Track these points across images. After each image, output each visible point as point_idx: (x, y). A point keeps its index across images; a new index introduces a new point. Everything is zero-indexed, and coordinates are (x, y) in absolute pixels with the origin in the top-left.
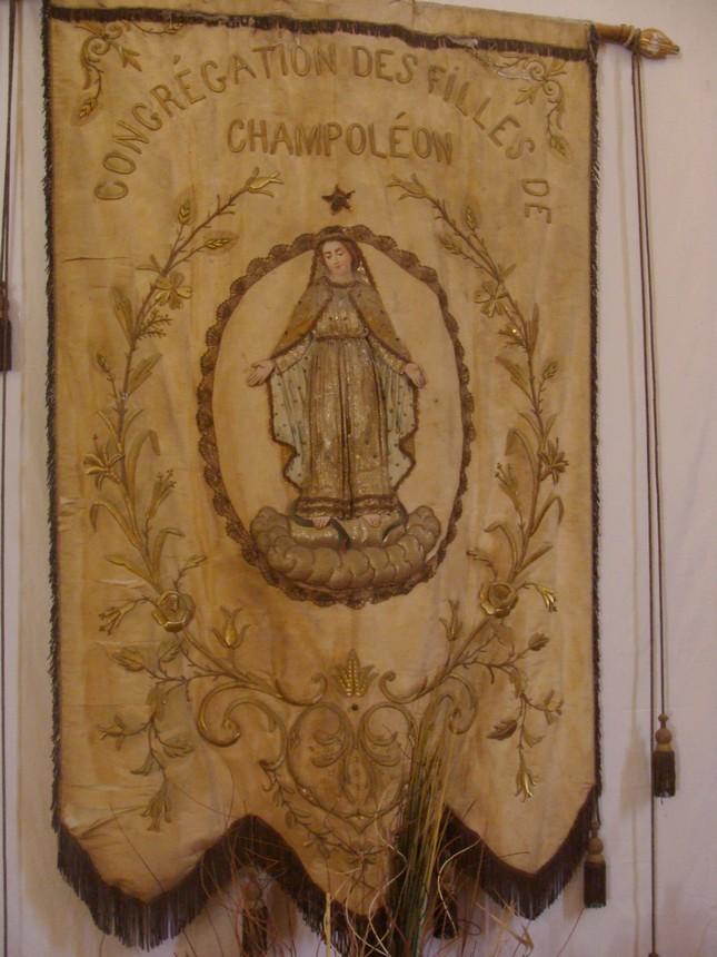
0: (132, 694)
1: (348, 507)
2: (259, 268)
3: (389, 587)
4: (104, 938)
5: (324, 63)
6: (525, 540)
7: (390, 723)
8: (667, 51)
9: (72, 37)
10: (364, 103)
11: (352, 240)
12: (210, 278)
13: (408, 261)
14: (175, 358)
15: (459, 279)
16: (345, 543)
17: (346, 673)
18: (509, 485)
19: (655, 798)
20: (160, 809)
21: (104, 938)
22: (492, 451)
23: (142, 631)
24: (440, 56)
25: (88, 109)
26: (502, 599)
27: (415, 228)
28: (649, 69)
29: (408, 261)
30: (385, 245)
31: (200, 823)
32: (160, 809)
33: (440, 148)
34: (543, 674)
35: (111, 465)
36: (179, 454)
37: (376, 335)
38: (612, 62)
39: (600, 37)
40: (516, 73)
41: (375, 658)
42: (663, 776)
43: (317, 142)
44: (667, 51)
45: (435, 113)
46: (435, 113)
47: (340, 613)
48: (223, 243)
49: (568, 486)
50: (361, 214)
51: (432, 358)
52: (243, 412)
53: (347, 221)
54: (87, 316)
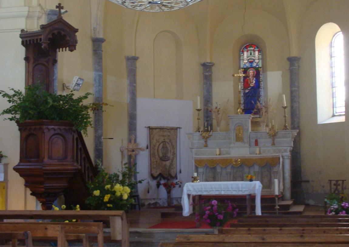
0: (155, 166)
1: (166, 156)
2: (161, 143)
3: (168, 160)
4: (135, 54)
5: (163, 131)
6: (173, 158)
7: (168, 168)
8: (181, 128)
9: (151, 130)
10: (165, 134)
11: (165, 142)
12: (158, 144)
13: (168, 143)
14: (156, 148)
15: (170, 143)
16: (165, 158)
17: (165, 165)
18: (173, 155)
19: (335, 181)
20: (156, 172)
21: (135, 54)
22: (172, 153)
23: (155, 163)
24: (169, 130)
25: (152, 134)
26: (172, 161)
27: (168, 141)
28: (181, 129)
29: (168, 143)
30: (167, 142)
31: (158, 173)
32: (156, 172)
33: (169, 136)
34: (174, 166)
35: (154, 154)
36: (156, 154)
37: (166, 147)
38: (178, 129)
39: (178, 128)
40: (173, 131)
41: (167, 164)
42: (180, 172)
43: (163, 136)
44: (181, 128)
45: (169, 134)
46: (169, 134)
47: (165, 162)
48: (158, 142)
49: (175, 155)
50: (165, 140)
51: (169, 148)
52: (160, 151)
53: (165, 141)
54: (152, 146)
